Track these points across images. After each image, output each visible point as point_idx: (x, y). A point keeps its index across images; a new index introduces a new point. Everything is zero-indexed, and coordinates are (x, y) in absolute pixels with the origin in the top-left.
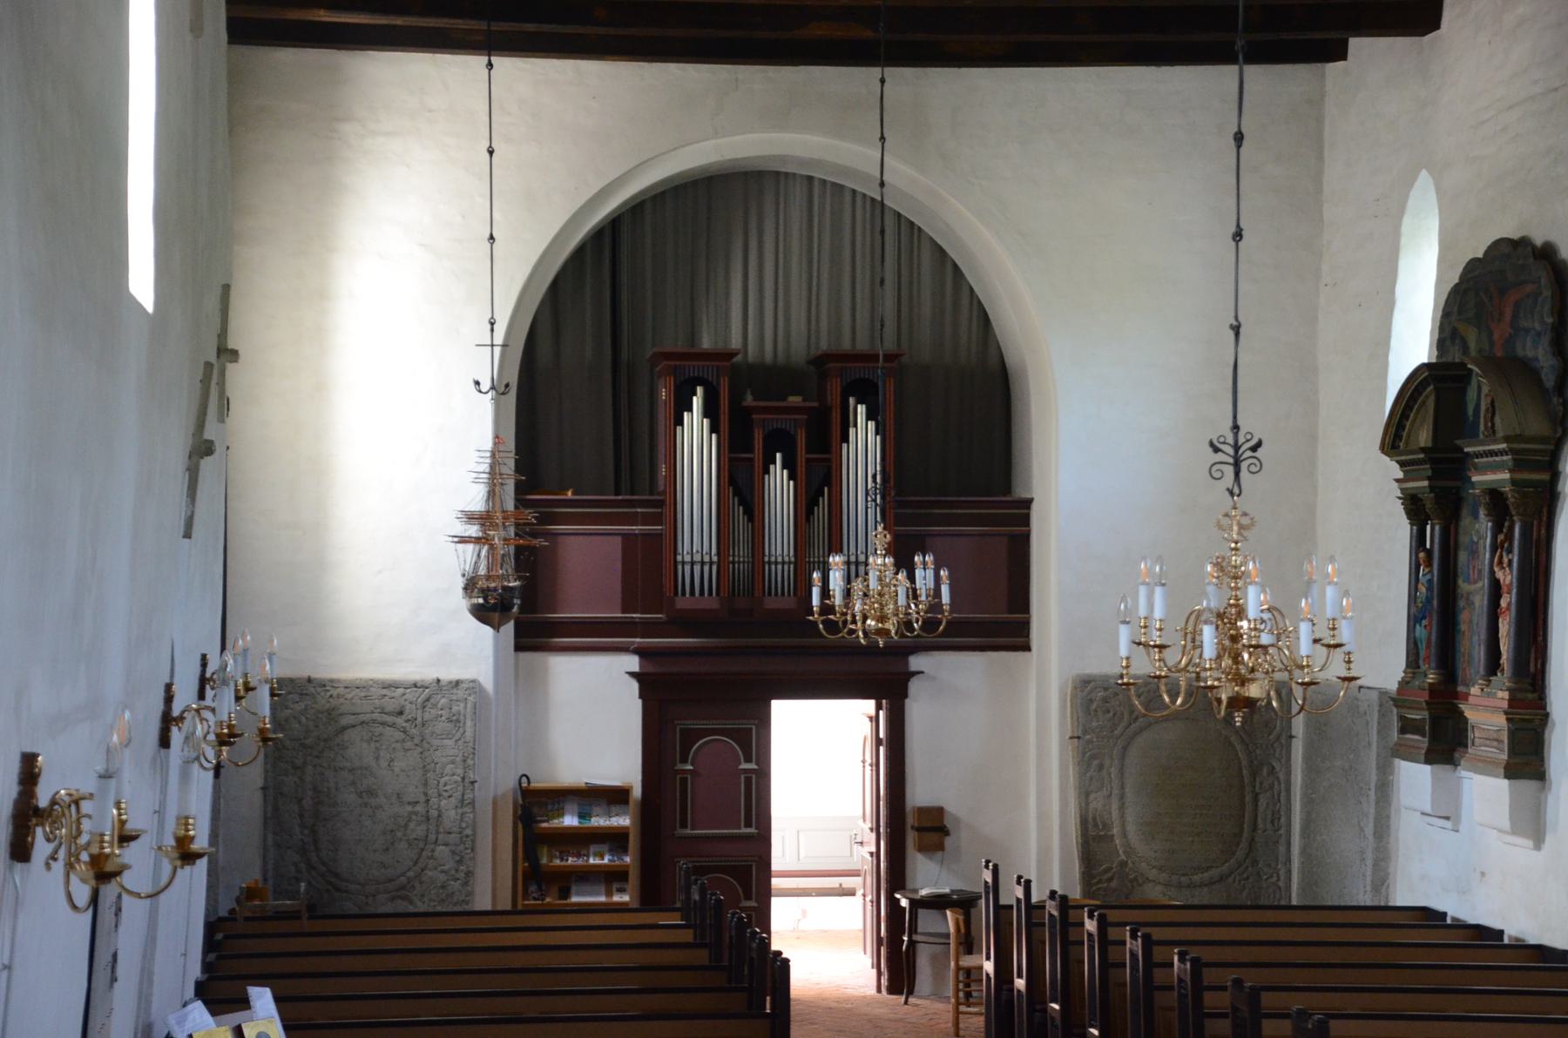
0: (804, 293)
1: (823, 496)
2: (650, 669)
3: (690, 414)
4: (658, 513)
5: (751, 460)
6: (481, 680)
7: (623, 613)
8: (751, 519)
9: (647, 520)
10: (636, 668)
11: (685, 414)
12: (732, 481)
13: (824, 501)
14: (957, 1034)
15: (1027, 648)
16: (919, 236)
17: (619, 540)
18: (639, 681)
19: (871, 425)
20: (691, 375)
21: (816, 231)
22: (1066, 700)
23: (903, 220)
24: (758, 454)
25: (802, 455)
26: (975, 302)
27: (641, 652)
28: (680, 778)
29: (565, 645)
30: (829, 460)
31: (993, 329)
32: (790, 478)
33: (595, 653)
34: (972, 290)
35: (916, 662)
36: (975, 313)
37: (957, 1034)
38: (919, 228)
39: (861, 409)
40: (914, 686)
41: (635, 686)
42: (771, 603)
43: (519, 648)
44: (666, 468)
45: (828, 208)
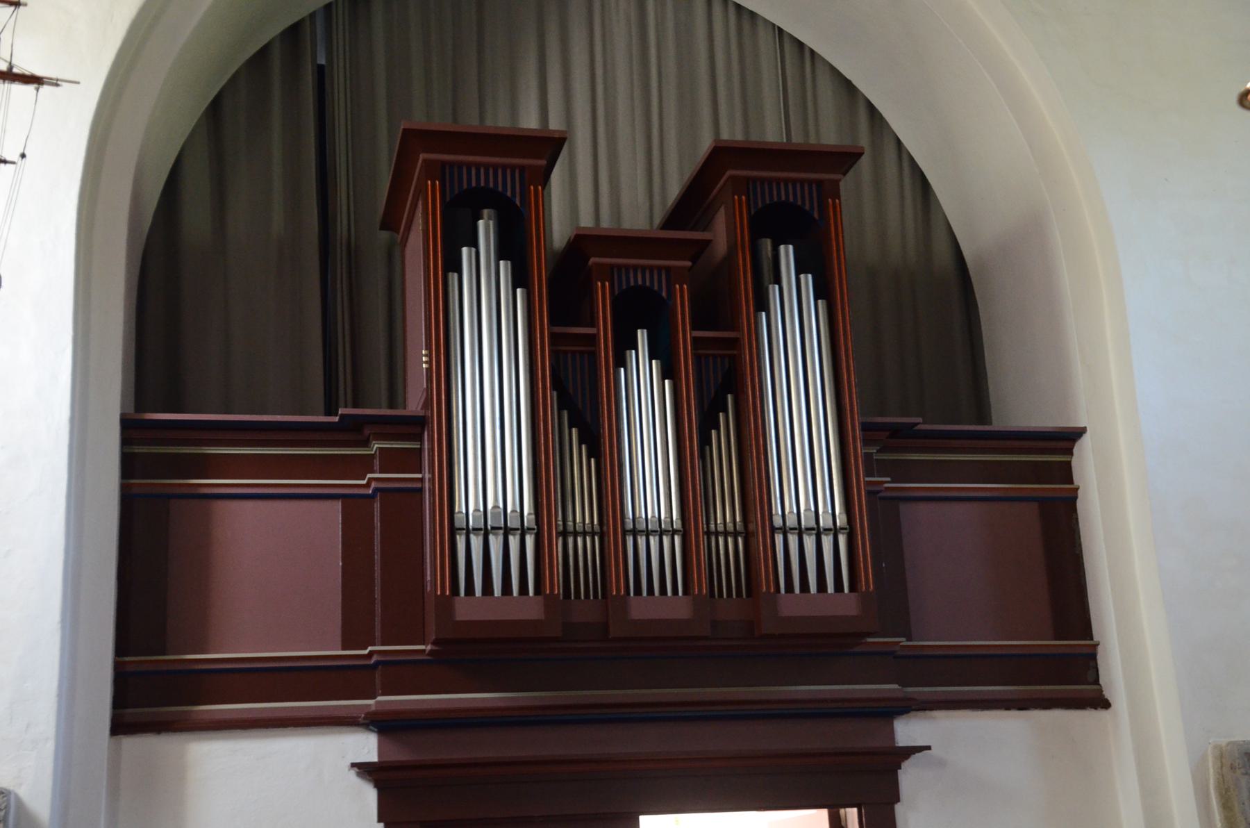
0: (641, 156)
1: (726, 411)
2: (400, 755)
3: (473, 250)
4: (418, 448)
5: (593, 339)
6: (23, 792)
7: (343, 649)
8: (595, 451)
9: (391, 461)
10: (373, 757)
11: (465, 250)
12: (558, 384)
13: (728, 421)
14: (9, 76)
15: (1102, 703)
16: (813, 64)
17: (338, 505)
18: (378, 785)
19: (808, 280)
20: (474, 184)
21: (653, 51)
22: (1207, 795)
23: (786, 39)
24: (604, 328)
25: (685, 334)
26: (905, 157)
27: (381, 724)
28: (425, 161)
29: (228, 717)
30: (735, 343)
31: (934, 195)
32: (664, 375)
33: (299, 730)
34: (899, 142)
35: (907, 731)
36: (907, 181)
37: (9, 76)
38: (812, 52)
39: (787, 254)
40: (909, 776)
41: (369, 795)
42: (640, 609)
43: (120, 727)
44: (429, 355)
45: (670, 24)
